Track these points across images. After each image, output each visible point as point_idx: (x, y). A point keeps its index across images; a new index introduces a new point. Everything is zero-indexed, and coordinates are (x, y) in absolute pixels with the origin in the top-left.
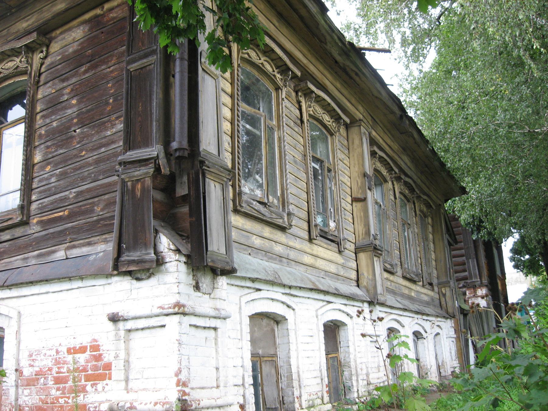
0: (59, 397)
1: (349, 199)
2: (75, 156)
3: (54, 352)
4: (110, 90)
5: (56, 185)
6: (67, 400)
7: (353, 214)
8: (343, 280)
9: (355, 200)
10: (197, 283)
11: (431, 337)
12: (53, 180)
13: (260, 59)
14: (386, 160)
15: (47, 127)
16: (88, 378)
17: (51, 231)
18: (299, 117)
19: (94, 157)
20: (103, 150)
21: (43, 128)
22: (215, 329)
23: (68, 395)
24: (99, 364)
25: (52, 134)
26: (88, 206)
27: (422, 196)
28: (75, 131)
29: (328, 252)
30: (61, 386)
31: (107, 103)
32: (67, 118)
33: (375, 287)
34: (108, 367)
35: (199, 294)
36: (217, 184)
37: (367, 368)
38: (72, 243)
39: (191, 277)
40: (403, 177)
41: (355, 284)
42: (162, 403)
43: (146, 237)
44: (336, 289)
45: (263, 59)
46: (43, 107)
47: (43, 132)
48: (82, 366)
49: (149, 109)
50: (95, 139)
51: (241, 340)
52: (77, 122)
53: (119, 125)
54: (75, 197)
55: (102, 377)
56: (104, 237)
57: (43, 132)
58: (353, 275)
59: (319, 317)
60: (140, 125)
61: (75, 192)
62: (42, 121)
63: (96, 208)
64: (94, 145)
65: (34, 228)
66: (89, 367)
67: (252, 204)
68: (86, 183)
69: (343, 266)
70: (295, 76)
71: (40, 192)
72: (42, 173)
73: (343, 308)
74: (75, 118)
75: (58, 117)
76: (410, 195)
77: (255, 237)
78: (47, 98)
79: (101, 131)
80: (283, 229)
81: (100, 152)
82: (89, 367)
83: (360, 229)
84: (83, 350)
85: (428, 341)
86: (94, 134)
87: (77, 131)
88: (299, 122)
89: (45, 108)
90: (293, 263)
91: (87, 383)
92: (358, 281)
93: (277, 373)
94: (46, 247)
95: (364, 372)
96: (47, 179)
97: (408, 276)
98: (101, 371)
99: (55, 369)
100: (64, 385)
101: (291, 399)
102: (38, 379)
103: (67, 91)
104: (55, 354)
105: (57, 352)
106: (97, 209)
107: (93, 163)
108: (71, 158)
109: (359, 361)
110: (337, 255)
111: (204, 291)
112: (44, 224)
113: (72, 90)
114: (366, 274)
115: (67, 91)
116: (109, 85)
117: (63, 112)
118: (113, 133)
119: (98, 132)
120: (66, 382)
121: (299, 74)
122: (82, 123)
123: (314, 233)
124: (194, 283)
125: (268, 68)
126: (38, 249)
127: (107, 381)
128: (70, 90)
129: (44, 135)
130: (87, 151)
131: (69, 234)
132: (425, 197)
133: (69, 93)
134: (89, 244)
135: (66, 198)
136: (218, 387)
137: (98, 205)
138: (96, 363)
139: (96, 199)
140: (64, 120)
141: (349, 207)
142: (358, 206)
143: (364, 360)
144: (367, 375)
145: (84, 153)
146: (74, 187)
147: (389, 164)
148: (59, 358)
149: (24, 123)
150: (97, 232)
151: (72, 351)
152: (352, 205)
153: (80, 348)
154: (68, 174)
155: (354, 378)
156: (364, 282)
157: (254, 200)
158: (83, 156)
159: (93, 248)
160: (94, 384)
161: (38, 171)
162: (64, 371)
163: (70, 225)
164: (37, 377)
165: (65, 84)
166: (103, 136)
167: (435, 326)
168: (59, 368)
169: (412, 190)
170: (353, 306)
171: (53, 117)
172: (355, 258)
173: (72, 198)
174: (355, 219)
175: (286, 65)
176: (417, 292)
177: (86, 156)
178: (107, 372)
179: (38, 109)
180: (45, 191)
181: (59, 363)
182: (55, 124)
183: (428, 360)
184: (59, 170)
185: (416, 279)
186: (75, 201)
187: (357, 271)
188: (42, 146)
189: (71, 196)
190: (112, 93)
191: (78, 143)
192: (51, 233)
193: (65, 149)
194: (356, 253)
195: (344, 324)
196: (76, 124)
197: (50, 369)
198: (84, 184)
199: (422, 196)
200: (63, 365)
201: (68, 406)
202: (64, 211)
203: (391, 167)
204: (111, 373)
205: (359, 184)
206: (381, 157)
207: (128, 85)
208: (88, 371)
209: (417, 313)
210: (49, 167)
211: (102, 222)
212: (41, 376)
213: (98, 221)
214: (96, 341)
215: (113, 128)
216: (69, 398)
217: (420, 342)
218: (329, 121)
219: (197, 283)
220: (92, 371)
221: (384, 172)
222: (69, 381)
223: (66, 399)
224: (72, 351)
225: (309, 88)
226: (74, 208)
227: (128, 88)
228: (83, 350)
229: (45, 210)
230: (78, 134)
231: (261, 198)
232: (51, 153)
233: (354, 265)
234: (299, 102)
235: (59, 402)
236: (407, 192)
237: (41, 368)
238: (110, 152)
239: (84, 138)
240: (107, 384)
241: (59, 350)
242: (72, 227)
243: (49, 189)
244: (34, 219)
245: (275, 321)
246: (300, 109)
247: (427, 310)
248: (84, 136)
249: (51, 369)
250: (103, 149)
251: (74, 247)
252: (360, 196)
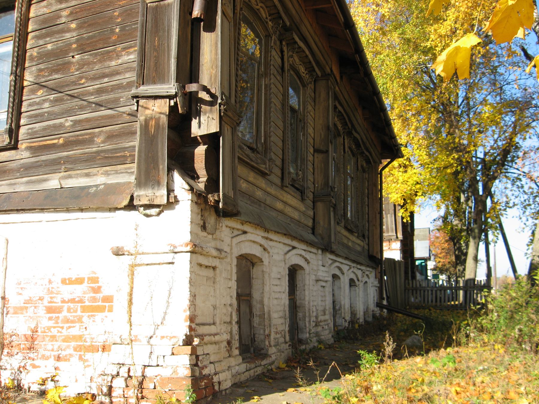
0: (51, 327)
1: (312, 150)
2: (73, 82)
3: (47, 282)
4: (117, 19)
5: (49, 111)
6: (60, 330)
7: (313, 165)
8: (303, 227)
9: (316, 151)
10: (204, 223)
11: (361, 285)
12: (47, 105)
13: (257, 5)
14: (343, 115)
15: (40, 49)
16: (84, 309)
17: (43, 158)
18: (281, 65)
19: (96, 87)
20: (106, 80)
21: (35, 49)
22: (214, 268)
23: (61, 325)
24: (98, 296)
25: (44, 57)
26: (87, 137)
27: (365, 152)
28: (73, 57)
29: (294, 199)
30: (54, 315)
31: (112, 31)
32: (65, 42)
33: (330, 236)
34: (108, 299)
35: (205, 234)
36: (229, 127)
37: (317, 310)
38: (67, 173)
39: (200, 216)
40: (354, 132)
41: (310, 231)
42: (169, 338)
43: (159, 175)
44: (301, 235)
45: (260, 4)
46: (36, 27)
47: (35, 54)
48: (78, 297)
49: (166, 45)
50: (97, 67)
51: (230, 279)
52: (76, 48)
53: (126, 56)
54: (72, 126)
55: (101, 309)
56: (105, 168)
57: (35, 54)
58: (310, 224)
59: (287, 261)
60: (155, 60)
61: (71, 121)
62: (34, 41)
63: (96, 139)
64: (96, 74)
65: (23, 153)
66: (86, 298)
67: (243, 149)
68: (85, 112)
69: (304, 213)
70: (284, 25)
71: (30, 117)
72: (33, 96)
73: (303, 253)
74: (74, 43)
75: (54, 40)
76: (355, 150)
77: (242, 181)
78: (42, 17)
79: (105, 61)
80: (263, 174)
81: (103, 82)
82: (86, 298)
83: (320, 179)
84: (79, 281)
85: (359, 288)
86: (96, 62)
87: (76, 57)
88: (280, 71)
89: (38, 29)
90: (268, 208)
91: (83, 314)
92: (313, 229)
93: (251, 312)
94: (37, 174)
95: (315, 314)
96: (38, 104)
97: (349, 227)
98: (100, 303)
99: (47, 299)
100: (57, 315)
101: (262, 337)
102: (26, 308)
103: (65, 13)
104: (48, 284)
105: (50, 282)
106: (98, 140)
107: (94, 92)
108: (68, 85)
109: (311, 304)
110: (300, 203)
111: (209, 231)
112: (35, 150)
113: (71, 13)
114: (322, 223)
115: (65, 13)
116: (115, 14)
117: (60, 35)
118: (118, 64)
119: (100, 61)
120: (60, 312)
121: (288, 24)
122: (82, 49)
123: (287, 181)
124: (202, 223)
125: (264, 14)
126: (27, 175)
127: (106, 313)
128: (69, 13)
129: (36, 57)
130: (87, 79)
131: (64, 163)
132: (367, 154)
133: (68, 16)
134: (87, 175)
135: (61, 126)
136: (214, 324)
137: (98, 137)
138: (94, 295)
139: (97, 130)
140: (60, 44)
141: (310, 158)
142: (319, 157)
143: (315, 303)
144: (317, 317)
145: (83, 81)
146: (71, 115)
147: (344, 119)
148: (52, 288)
149: (12, 42)
150: (96, 164)
151: (67, 282)
152: (313, 156)
153: (77, 279)
154: (65, 101)
155: (307, 319)
156: (320, 230)
157: (245, 145)
158: (83, 84)
159: (91, 180)
160: (92, 316)
161: (28, 94)
162: (57, 301)
163: (65, 154)
164: (26, 305)
165: (63, 6)
166: (107, 66)
167: (365, 276)
168: (51, 298)
169: (358, 145)
170: (310, 252)
171: (48, 39)
172: (312, 207)
173: (68, 126)
174: (316, 170)
175: (279, 13)
176: (353, 242)
177: (86, 85)
178: (107, 304)
179: (30, 29)
180: (36, 116)
181: (52, 293)
182: (49, 47)
183: (358, 306)
184: (53, 96)
185: (355, 230)
186: (71, 130)
187: (314, 220)
188: (34, 68)
189: (67, 124)
190: (119, 22)
191: (77, 70)
192: (43, 161)
193: (61, 74)
194: (314, 202)
195: (301, 268)
196: (75, 50)
197: (41, 299)
198: (83, 113)
199: (365, 152)
200: (57, 295)
201: (61, 336)
202: (59, 138)
203: (346, 122)
204: (112, 306)
205: (323, 136)
206: (340, 112)
207: (143, 16)
208: (85, 302)
209: (354, 261)
210: (42, 91)
211: (102, 154)
212: (30, 305)
213: (98, 152)
214: (95, 273)
215: (118, 59)
216: (62, 328)
217: (353, 288)
218: (304, 73)
219: (204, 223)
220: (89, 302)
221: (340, 126)
222: (63, 311)
223: (59, 329)
224: (67, 282)
225: (294, 39)
226: (70, 136)
227: (144, 20)
228: (79, 281)
229: (36, 136)
230: (77, 62)
231: (251, 143)
232: (44, 76)
233: (311, 213)
234: (282, 51)
235: (51, 332)
236: (354, 147)
237: (30, 297)
238: (114, 83)
239: (84, 65)
240: (106, 317)
241: (52, 280)
242: (67, 157)
243: (42, 115)
244: (22, 144)
245: (252, 262)
246: (282, 59)
247: (361, 260)
248: (82, 64)
249: (43, 299)
250: (107, 79)
251: (70, 177)
252: (322, 148)
